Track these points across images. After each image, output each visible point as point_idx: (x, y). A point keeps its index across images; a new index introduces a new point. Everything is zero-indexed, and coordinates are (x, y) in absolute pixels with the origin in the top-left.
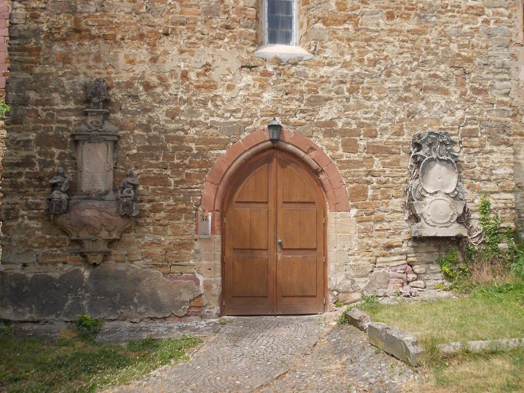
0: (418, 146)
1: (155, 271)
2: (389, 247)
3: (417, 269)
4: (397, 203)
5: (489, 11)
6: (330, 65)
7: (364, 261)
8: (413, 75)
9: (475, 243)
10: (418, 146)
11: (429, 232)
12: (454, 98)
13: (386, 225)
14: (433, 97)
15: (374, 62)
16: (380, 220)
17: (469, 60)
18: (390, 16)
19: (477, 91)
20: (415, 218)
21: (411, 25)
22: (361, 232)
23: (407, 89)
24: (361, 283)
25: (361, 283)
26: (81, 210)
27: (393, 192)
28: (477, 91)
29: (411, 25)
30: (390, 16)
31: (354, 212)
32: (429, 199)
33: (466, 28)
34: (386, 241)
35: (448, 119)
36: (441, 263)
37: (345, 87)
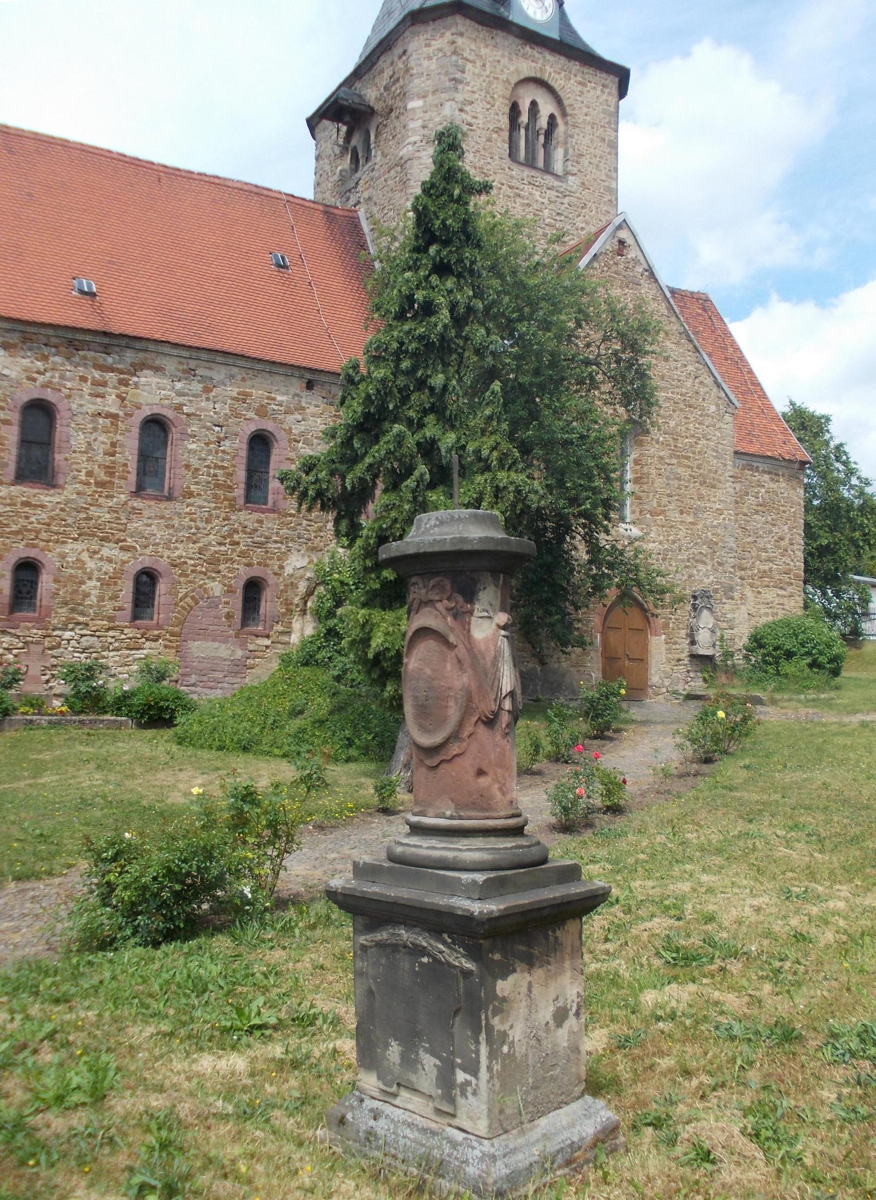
0: (695, 598)
1: (572, 669)
2: (679, 660)
3: (692, 674)
4: (683, 633)
5: (725, 512)
6: (654, 542)
7: (668, 668)
8: (691, 551)
9: (718, 660)
10: (695, 598)
11: (702, 652)
12: (709, 568)
13: (678, 646)
14: (700, 566)
15: (674, 542)
16: (675, 643)
17: (716, 544)
18: (682, 512)
19: (720, 564)
20: (693, 643)
21: (690, 519)
22: (667, 649)
23: (688, 561)
24: (667, 682)
25: (667, 682)
26: (158, 1034)
27: (681, 626)
28: (720, 564)
29: (690, 519)
30: (682, 512)
31: (663, 637)
32: (701, 631)
33: (715, 523)
34: (677, 656)
35: (706, 581)
36: (701, 672)
37: (661, 557)
